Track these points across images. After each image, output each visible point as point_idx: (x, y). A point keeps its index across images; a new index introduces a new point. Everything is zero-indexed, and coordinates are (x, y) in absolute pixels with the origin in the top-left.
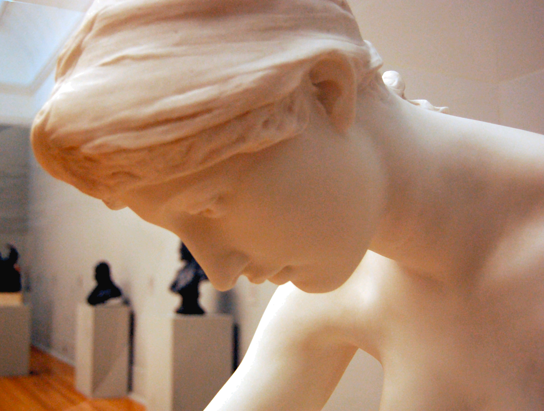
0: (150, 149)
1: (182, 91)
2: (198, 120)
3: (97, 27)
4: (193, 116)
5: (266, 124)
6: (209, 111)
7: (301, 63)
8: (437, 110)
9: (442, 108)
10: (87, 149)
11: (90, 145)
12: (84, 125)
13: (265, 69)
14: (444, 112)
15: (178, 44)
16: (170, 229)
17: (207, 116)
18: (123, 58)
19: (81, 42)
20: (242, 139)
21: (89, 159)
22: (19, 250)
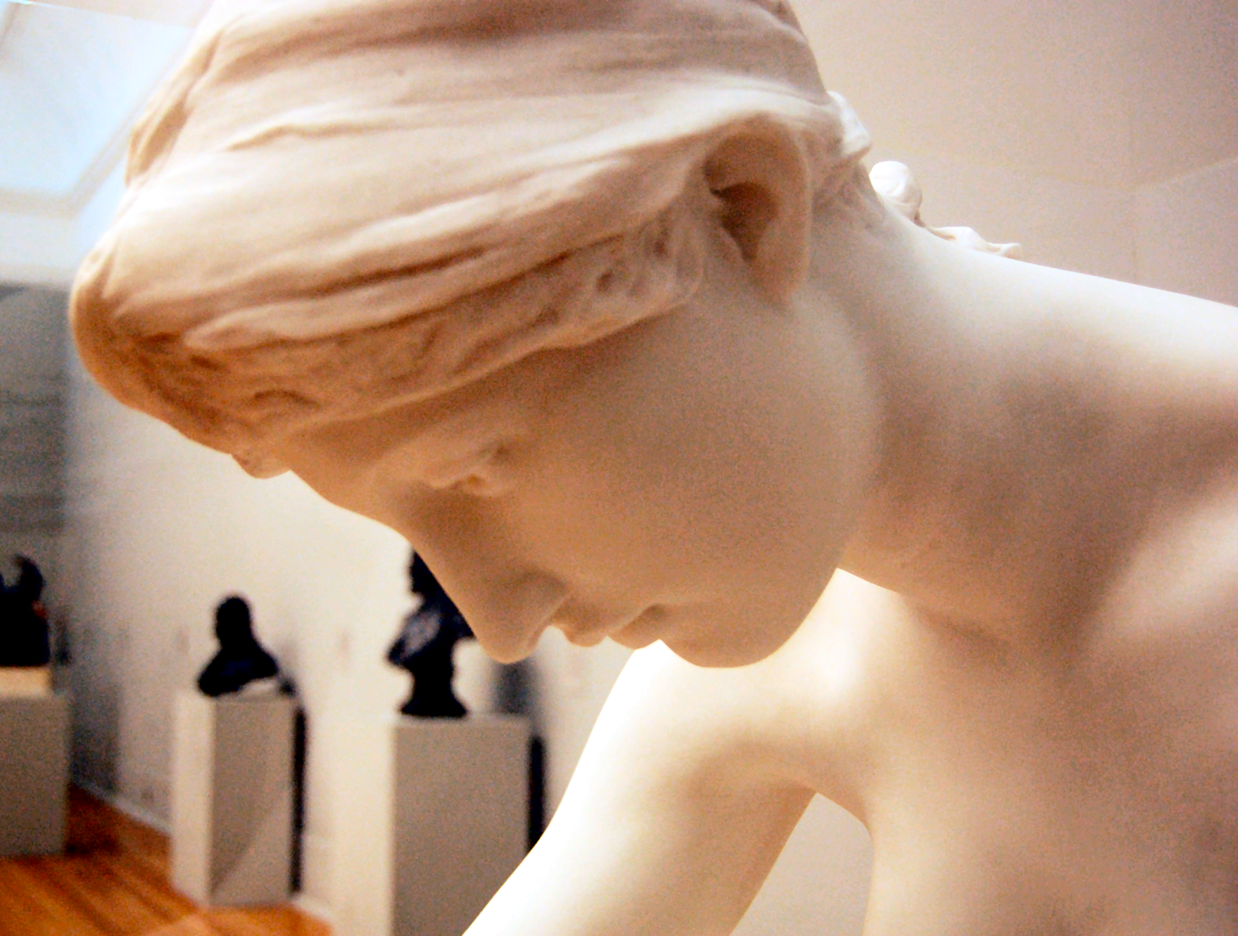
0: (342, 339)
1: (414, 206)
2: (450, 272)
3: (221, 61)
4: (440, 264)
5: (605, 281)
6: (475, 252)
7: (684, 144)
8: (995, 250)
9: (1005, 247)
10: (198, 340)
11: (205, 330)
12: (190, 284)
13: (604, 157)
14: (1010, 255)
15: (404, 101)
16: (388, 523)
17: (471, 265)
18: (280, 132)
19: (185, 95)
20: (550, 316)
21: (202, 362)
22: (44, 568)
